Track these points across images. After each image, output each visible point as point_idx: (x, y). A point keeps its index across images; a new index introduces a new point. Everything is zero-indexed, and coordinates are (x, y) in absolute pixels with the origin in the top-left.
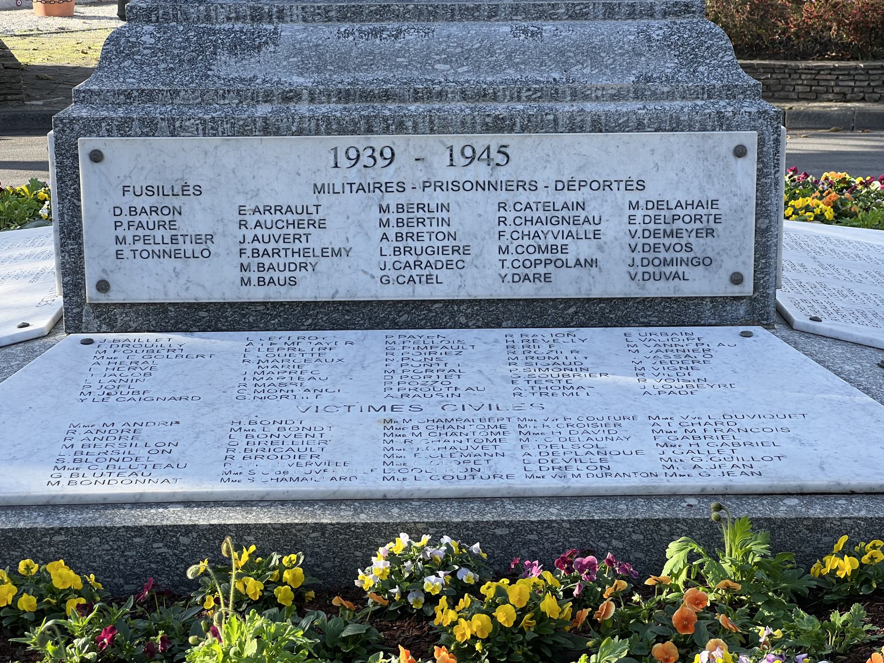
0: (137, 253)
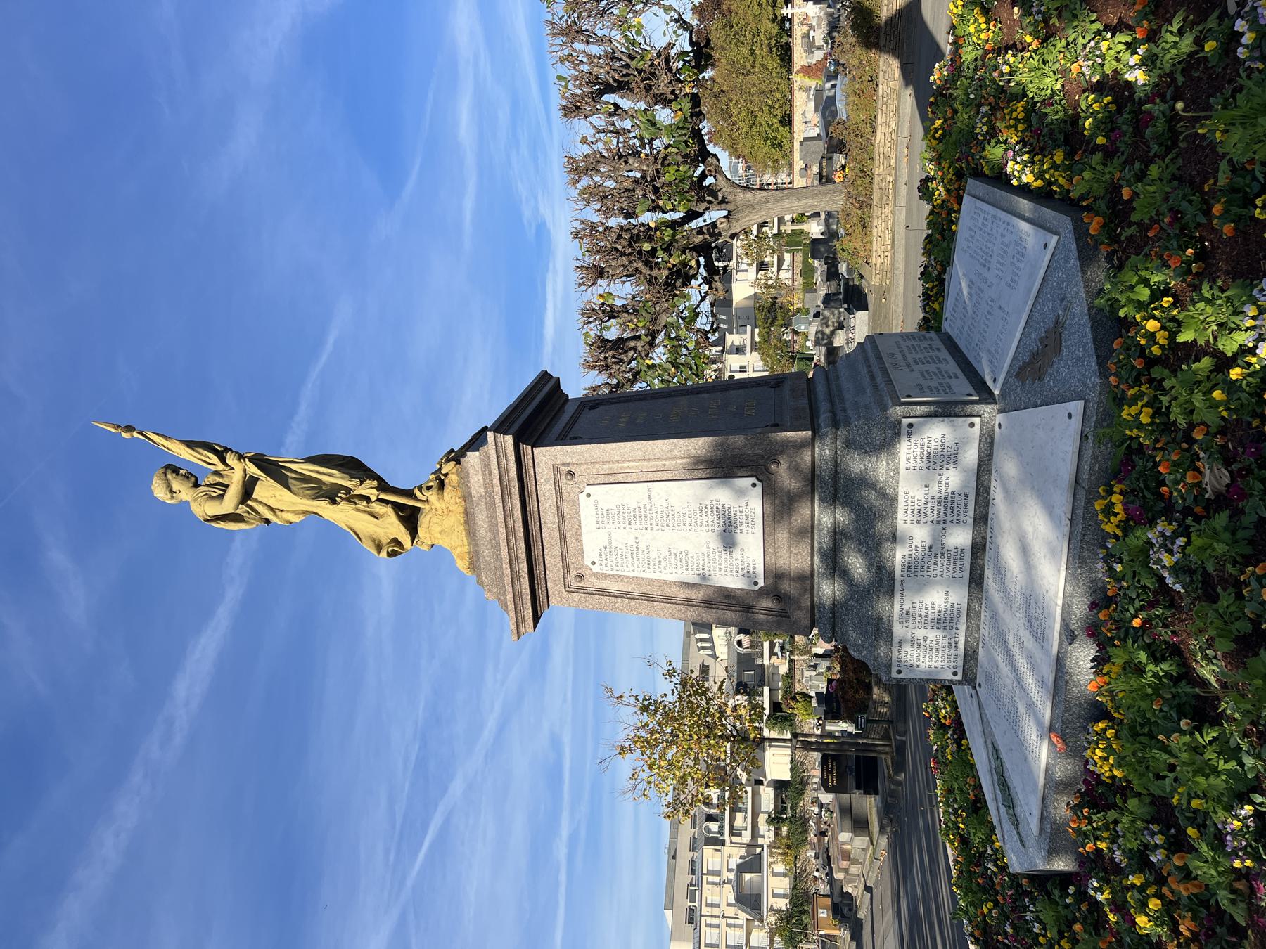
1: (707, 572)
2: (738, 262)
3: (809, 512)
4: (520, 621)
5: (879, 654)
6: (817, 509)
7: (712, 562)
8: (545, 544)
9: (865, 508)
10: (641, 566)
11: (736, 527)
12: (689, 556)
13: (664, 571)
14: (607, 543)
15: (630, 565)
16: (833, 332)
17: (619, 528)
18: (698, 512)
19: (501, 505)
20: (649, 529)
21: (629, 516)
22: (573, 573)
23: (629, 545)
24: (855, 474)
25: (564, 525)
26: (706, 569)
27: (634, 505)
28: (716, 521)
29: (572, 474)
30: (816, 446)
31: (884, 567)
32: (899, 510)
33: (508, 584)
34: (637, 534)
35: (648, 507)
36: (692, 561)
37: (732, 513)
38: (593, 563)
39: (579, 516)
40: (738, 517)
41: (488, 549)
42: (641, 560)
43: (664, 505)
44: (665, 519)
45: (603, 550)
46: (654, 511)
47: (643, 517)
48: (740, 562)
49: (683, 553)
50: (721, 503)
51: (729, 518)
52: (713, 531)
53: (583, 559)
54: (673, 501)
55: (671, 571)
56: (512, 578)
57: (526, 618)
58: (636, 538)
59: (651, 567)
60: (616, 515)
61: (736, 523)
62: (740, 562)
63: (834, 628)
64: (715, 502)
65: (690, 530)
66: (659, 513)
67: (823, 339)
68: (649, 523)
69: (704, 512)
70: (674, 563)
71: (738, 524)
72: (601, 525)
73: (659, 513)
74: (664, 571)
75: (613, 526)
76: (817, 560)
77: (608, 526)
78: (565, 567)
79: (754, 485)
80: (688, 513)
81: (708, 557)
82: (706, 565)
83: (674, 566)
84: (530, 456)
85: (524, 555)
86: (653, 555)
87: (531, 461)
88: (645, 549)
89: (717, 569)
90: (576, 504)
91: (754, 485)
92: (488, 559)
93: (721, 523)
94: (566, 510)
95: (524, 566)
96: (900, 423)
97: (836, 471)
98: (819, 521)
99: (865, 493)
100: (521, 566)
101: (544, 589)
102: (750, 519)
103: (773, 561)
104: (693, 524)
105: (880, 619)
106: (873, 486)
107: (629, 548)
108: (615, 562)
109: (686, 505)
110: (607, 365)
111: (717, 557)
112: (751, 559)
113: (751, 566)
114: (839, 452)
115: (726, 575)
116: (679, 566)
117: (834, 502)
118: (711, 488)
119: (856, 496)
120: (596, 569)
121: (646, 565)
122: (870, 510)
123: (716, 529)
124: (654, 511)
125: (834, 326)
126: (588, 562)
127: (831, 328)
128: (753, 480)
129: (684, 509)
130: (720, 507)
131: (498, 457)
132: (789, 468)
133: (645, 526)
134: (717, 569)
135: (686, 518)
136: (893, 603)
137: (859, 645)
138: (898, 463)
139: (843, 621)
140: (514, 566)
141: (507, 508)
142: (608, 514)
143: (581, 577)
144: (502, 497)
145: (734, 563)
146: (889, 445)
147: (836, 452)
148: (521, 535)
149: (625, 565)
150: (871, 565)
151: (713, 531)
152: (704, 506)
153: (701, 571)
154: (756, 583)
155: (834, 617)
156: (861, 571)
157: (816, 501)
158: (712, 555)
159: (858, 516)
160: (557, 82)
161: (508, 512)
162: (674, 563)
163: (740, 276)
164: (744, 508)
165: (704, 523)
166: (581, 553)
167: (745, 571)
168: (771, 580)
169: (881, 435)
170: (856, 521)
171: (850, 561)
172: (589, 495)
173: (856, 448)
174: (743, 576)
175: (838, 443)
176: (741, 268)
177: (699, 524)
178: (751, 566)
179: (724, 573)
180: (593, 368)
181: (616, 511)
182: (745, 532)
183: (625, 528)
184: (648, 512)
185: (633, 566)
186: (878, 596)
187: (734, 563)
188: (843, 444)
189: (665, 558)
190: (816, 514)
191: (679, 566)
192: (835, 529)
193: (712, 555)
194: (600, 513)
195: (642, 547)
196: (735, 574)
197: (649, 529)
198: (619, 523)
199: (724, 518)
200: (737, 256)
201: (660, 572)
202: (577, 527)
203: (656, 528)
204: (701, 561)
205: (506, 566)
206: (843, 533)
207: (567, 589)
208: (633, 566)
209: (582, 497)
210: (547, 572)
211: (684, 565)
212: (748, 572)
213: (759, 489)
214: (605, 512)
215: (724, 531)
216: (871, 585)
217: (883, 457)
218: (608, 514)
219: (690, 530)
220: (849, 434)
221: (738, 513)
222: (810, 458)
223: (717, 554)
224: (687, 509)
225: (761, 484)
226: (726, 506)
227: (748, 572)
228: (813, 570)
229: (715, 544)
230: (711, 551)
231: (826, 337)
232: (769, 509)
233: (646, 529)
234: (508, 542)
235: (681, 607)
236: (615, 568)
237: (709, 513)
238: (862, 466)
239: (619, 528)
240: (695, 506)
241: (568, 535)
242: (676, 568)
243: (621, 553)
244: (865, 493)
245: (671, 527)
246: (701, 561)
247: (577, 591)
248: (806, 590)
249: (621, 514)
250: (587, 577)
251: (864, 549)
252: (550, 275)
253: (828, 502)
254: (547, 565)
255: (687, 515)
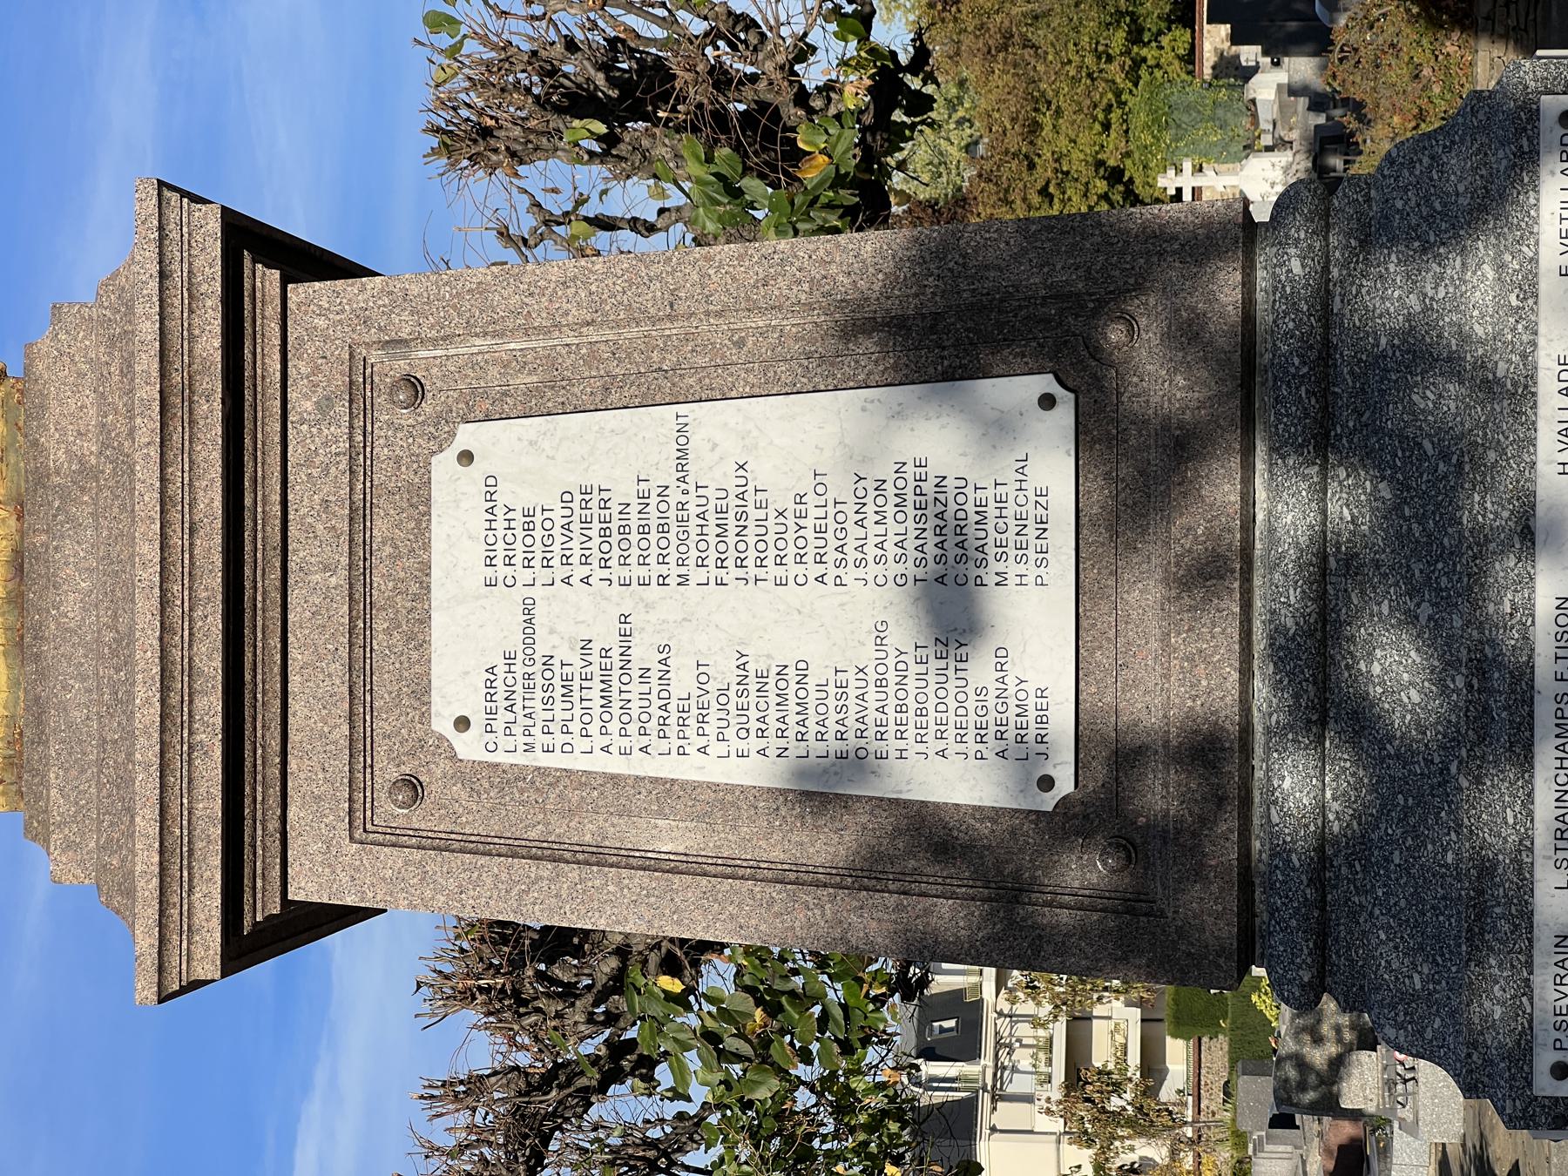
0: (624, 688)
1: (874, 746)
2: (999, 1068)
3: (1235, 498)
4: (173, 926)
5: (1485, 1018)
6: (1261, 494)
7: (892, 702)
8: (293, 653)
9: (1425, 456)
10: (633, 728)
11: (982, 563)
12: (811, 682)
13: (717, 749)
14: (515, 642)
15: (594, 729)
16: (1338, 1064)
17: (566, 581)
18: (850, 508)
19: (154, 452)
20: (673, 581)
21: (605, 534)
22: (387, 772)
23: (596, 647)
24: (1392, 333)
25: (368, 585)
26: (870, 733)
27: (624, 491)
28: (911, 544)
29: (415, 388)
30: (1260, 260)
31: (1497, 662)
32: (1541, 425)
33: (146, 904)
34: (625, 601)
35: (675, 497)
36: (822, 702)
37: (970, 508)
38: (462, 723)
39: (427, 547)
40: (990, 527)
41: (83, 678)
42: (635, 706)
43: (731, 484)
44: (731, 539)
45: (501, 670)
46: (693, 510)
47: (654, 536)
48: (991, 701)
49: (791, 671)
50: (933, 471)
51: (960, 530)
52: (900, 581)
53: (425, 717)
54: (761, 473)
55: (742, 745)
56: (164, 747)
57: (199, 918)
58: (624, 619)
59: (672, 731)
60: (557, 531)
61: (981, 549)
62: (991, 701)
63: (1321, 949)
64: (910, 469)
65: (820, 579)
66: (712, 517)
67: (1302, 1086)
68: (672, 559)
69: (870, 509)
70: (753, 714)
71: (991, 550)
72: (503, 571)
73: (712, 517)
74: (717, 749)
75: (544, 575)
76: (1261, 689)
77: (525, 576)
78: (359, 746)
79: (1047, 402)
80: (814, 512)
81: (881, 684)
82: (872, 716)
83: (754, 725)
84: (273, 310)
85: (218, 662)
86: (683, 683)
87: (275, 328)
88: (652, 658)
89: (911, 732)
90: (419, 500)
91: (1047, 402)
92: (77, 715)
93: (931, 550)
94: (381, 528)
95: (211, 705)
96: (1534, 114)
97: (1326, 343)
98: (1271, 531)
99: (1424, 399)
100: (201, 703)
101: (273, 825)
102: (1031, 531)
103: (1108, 699)
104: (832, 556)
105: (1486, 869)
106: (1452, 364)
107: (595, 658)
108: (541, 715)
109: (807, 485)
110: (516, 993)
111: (911, 684)
112: (1030, 687)
113: (1032, 714)
114: (1335, 272)
115: (942, 753)
116: (773, 725)
117: (1323, 723)
118: (898, 414)
119: (1393, 418)
120: (469, 747)
121: (653, 726)
122: (1445, 456)
123: (911, 570)
124: (693, 510)
125: (1340, 1040)
126: (442, 724)
127: (1332, 1049)
128: (1044, 383)
129: (800, 499)
130: (928, 487)
131: (163, 275)
132: (1167, 337)
133: (657, 569)
134: (911, 732)
135: (809, 533)
136: (1530, 795)
137: (1415, 996)
138: (1534, 260)
139: (1353, 916)
140: (174, 699)
141: (174, 471)
142: (528, 528)
143: (413, 787)
144: (163, 425)
145: (971, 704)
146: (1502, 196)
147: (1326, 269)
148: (212, 581)
149: (575, 727)
150: (1450, 664)
151: (900, 581)
152: (870, 485)
153: (853, 742)
154: (1047, 783)
155: (1322, 904)
156: (1416, 697)
157: (1260, 466)
158: (892, 677)
159: (1402, 487)
160: (422, 33)
161: (174, 489)
162: (753, 714)
163: (1007, 1114)
164: (1011, 489)
165: (871, 551)
166: (421, 692)
167: (1011, 734)
168: (1099, 772)
169: (1475, 170)
170: (1397, 508)
171: (1376, 669)
172: (466, 457)
173: (1393, 240)
174: (1001, 754)
175: (1333, 240)
176: (1010, 1089)
177: (852, 555)
178: (1032, 714)
179: (934, 745)
180: (467, 997)
181: (558, 515)
182: (1012, 580)
183: (585, 580)
184: (672, 514)
185: (604, 732)
186: (1478, 781)
187: (971, 704)
188: (1349, 235)
189: (723, 692)
190: (1260, 517)
191: (773, 725)
192: (1324, 558)
193: (892, 677)
194: (500, 525)
195: (644, 655)
196: (973, 747)
197: (673, 581)
198: (566, 560)
199: (940, 531)
200: (998, 1044)
201: (702, 750)
202: (414, 588)
203: (698, 575)
204: (852, 702)
205: (146, 696)
206: (1350, 563)
207: (358, 834)
208: (604, 732)
209: (444, 466)
210: (293, 765)
211: (792, 719)
212: (1021, 740)
213: (1064, 415)
214: (518, 521)
215: (940, 580)
216: (1450, 743)
217: (1483, 248)
218: (528, 528)
219: (820, 579)
220: (1368, 200)
221: (992, 511)
222: (1237, 295)
223: (914, 668)
224: (811, 499)
225: (1071, 396)
226: (950, 483)
227: (1021, 740)
228: (1246, 729)
229: (905, 633)
230: (891, 662)
231: (1312, 1079)
232: (1098, 496)
233: (663, 581)
234: (164, 603)
235: (774, 891)
236: (540, 739)
237: (890, 510)
238: (1413, 301)
239: (566, 581)
240: (840, 487)
241: (380, 625)
242: (761, 733)
243: (567, 680)
244: (1424, 399)
245: (753, 571)
246: (852, 702)
247: (395, 839)
248: (1221, 801)
249: (575, 527)
250: (433, 789)
251: (1426, 610)
252: (313, 1109)
253: (1299, 449)
254: (294, 737)
255: (809, 523)
